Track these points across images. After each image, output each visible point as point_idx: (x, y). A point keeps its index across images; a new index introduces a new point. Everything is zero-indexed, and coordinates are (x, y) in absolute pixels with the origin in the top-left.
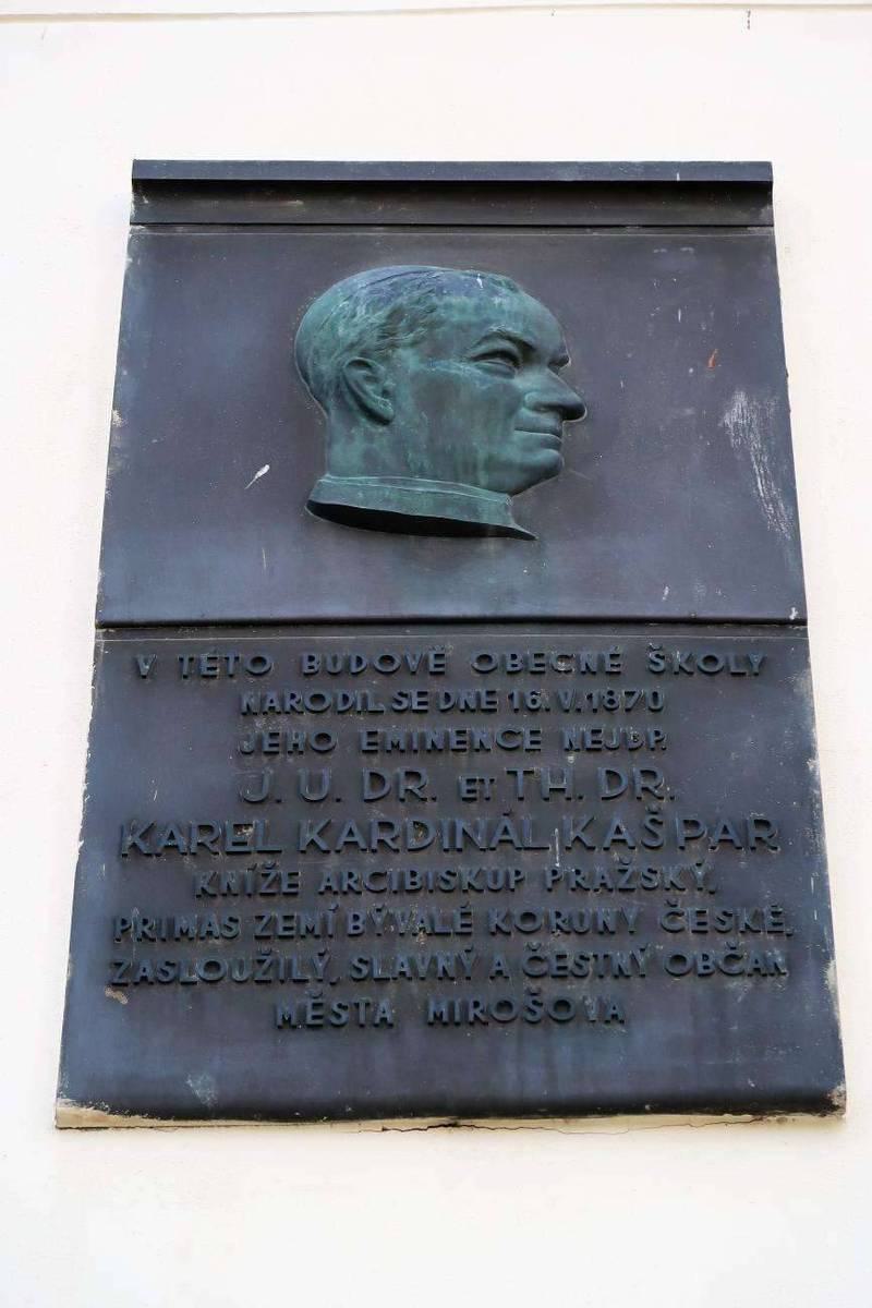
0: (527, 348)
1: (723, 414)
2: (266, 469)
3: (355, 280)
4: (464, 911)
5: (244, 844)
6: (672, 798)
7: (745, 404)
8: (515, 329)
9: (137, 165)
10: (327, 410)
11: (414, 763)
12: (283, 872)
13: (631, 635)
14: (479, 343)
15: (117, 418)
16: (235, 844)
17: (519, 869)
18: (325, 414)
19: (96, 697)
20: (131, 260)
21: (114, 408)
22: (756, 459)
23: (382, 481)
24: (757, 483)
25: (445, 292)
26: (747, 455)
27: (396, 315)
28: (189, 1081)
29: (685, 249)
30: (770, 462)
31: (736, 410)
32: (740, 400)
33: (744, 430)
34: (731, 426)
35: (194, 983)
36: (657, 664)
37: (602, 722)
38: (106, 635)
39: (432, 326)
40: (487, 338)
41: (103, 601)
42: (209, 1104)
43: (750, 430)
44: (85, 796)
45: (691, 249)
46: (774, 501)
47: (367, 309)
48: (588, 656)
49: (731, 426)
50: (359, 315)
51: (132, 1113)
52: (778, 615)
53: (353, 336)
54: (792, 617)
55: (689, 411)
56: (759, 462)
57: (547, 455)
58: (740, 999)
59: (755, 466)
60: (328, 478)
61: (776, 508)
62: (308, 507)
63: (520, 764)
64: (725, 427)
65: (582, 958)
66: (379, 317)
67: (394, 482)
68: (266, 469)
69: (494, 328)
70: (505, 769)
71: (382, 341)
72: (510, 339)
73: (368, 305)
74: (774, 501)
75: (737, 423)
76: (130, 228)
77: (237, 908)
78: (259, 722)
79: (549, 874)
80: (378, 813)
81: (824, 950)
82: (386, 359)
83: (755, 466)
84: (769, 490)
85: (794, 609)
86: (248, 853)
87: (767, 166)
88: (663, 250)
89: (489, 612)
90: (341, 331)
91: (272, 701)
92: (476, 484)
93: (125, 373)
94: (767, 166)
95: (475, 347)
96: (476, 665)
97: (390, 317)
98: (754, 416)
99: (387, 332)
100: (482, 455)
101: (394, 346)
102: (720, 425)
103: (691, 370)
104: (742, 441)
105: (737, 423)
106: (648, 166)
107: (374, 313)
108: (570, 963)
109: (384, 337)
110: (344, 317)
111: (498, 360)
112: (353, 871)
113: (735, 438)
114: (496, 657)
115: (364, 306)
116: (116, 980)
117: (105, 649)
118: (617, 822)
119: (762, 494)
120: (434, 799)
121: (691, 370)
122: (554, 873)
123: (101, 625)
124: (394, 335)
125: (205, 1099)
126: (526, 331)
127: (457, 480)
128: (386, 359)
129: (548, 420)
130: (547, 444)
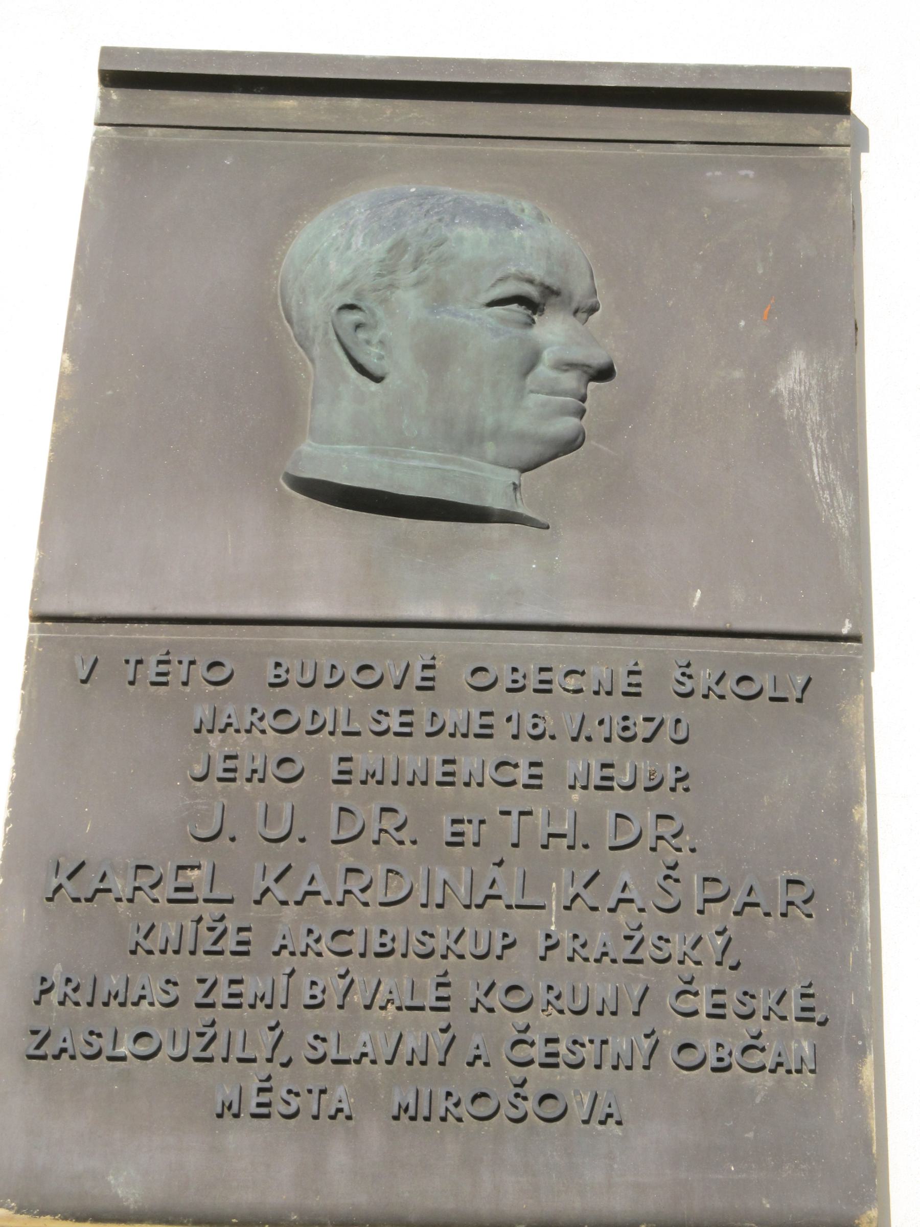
0: (550, 292)
1: (776, 377)
2: (698, 594)
3: (353, 203)
4: (442, 980)
5: (190, 889)
6: (693, 850)
7: (804, 366)
8: (538, 272)
9: (107, 53)
10: (312, 360)
11: (390, 796)
12: (231, 926)
13: (113, 632)
14: (493, 286)
15: (67, 363)
16: (177, 890)
17: (506, 931)
18: (309, 363)
19: (27, 703)
20: (92, 168)
21: (64, 351)
22: (813, 436)
23: (372, 452)
24: (811, 464)
25: (457, 221)
26: (802, 427)
27: (399, 248)
28: (111, 1177)
29: (743, 172)
30: (829, 439)
31: (793, 374)
32: (798, 361)
33: (800, 399)
34: (785, 394)
35: (123, 1059)
36: (682, 684)
37: (615, 751)
38: (40, 630)
39: (442, 261)
40: (502, 280)
41: (40, 587)
42: (132, 1207)
43: (808, 398)
44: (7, 824)
45: (751, 173)
46: (831, 488)
47: (364, 241)
48: (599, 672)
49: (785, 394)
50: (354, 246)
51: (42, 1213)
52: (831, 630)
53: (347, 272)
54: (845, 631)
55: (738, 374)
56: (817, 439)
57: (566, 425)
58: (758, 1100)
59: (811, 444)
60: (310, 445)
61: (833, 494)
62: (283, 479)
63: (516, 799)
64: (778, 394)
65: (575, 1042)
66: (379, 250)
67: (385, 454)
68: (698, 594)
69: (513, 270)
70: (498, 809)
71: (379, 280)
72: (531, 281)
73: (365, 235)
74: (831, 488)
75: (793, 389)
76: (93, 128)
77: (175, 966)
78: (215, 740)
79: (541, 938)
80: (346, 856)
81: (860, 1043)
82: (384, 301)
83: (811, 444)
84: (826, 473)
85: (847, 621)
86: (195, 901)
87: (845, 74)
88: (718, 173)
89: (488, 616)
90: (333, 265)
91: (229, 717)
92: (482, 458)
93: (79, 308)
94: (845, 74)
95: (488, 290)
96: (470, 680)
97: (390, 250)
98: (814, 382)
99: (388, 267)
100: (490, 421)
101: (392, 286)
102: (773, 391)
103: (742, 323)
104: (798, 413)
105: (793, 389)
106: (705, 70)
107: (372, 245)
108: (562, 1048)
109: (380, 275)
110: (337, 249)
111: (514, 306)
112: (313, 927)
113: (790, 407)
114: (493, 670)
115: (362, 236)
116: (32, 1052)
117: (39, 646)
118: (626, 877)
119: (817, 478)
120: (414, 842)
121: (742, 323)
122: (548, 936)
123: (39, 618)
124: (393, 272)
125: (128, 1199)
126: (549, 273)
127: (460, 452)
128: (384, 301)
129: (570, 380)
130: (564, 411)
